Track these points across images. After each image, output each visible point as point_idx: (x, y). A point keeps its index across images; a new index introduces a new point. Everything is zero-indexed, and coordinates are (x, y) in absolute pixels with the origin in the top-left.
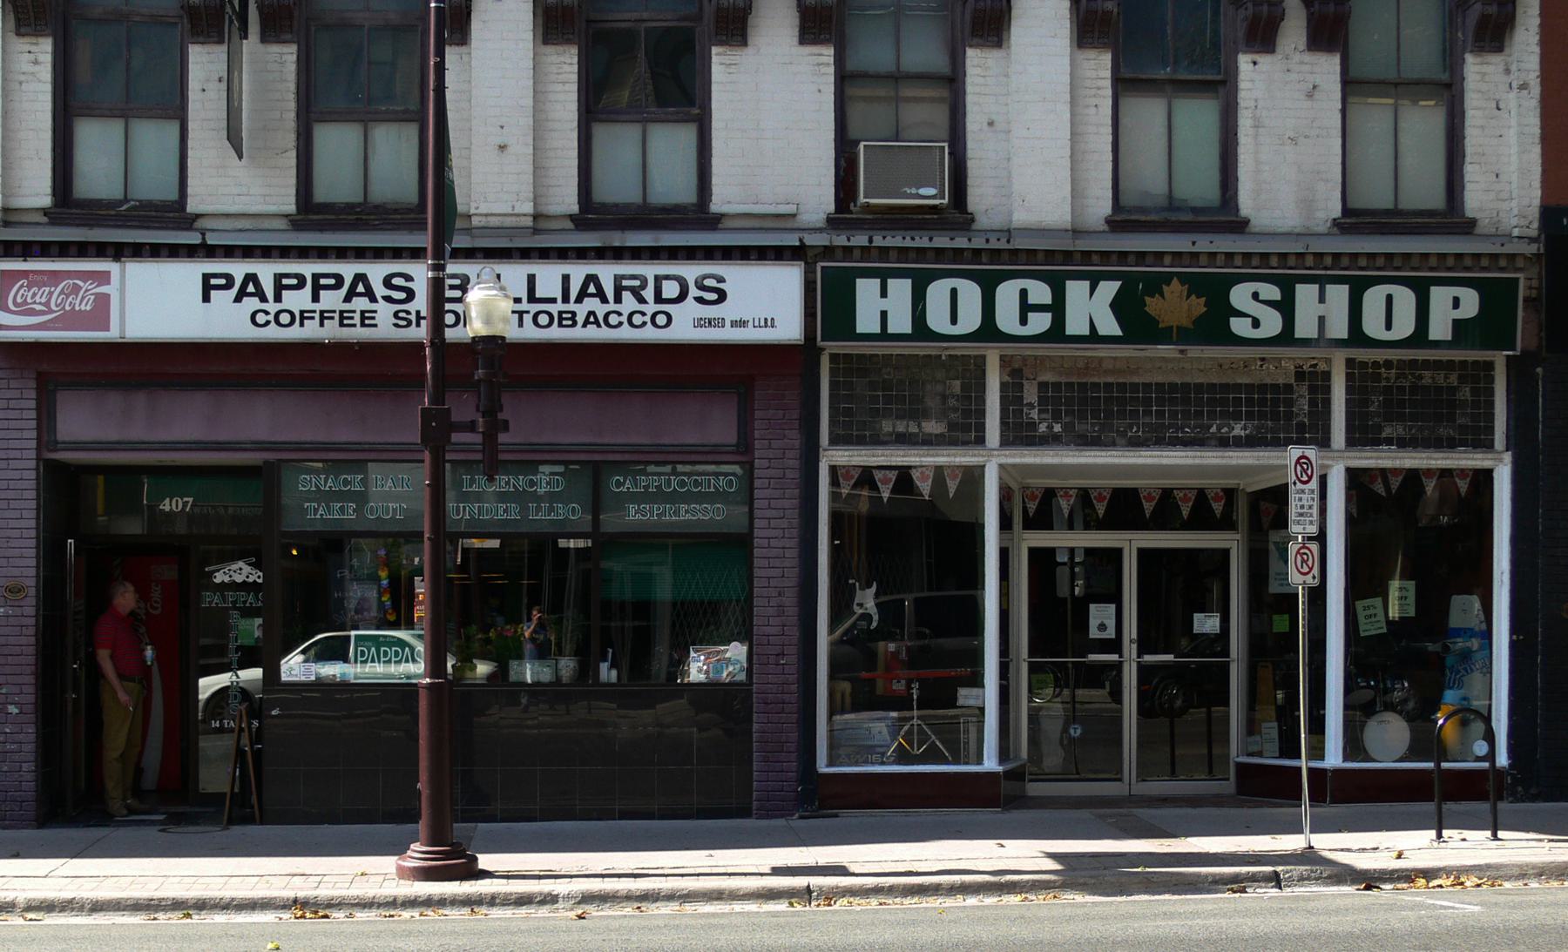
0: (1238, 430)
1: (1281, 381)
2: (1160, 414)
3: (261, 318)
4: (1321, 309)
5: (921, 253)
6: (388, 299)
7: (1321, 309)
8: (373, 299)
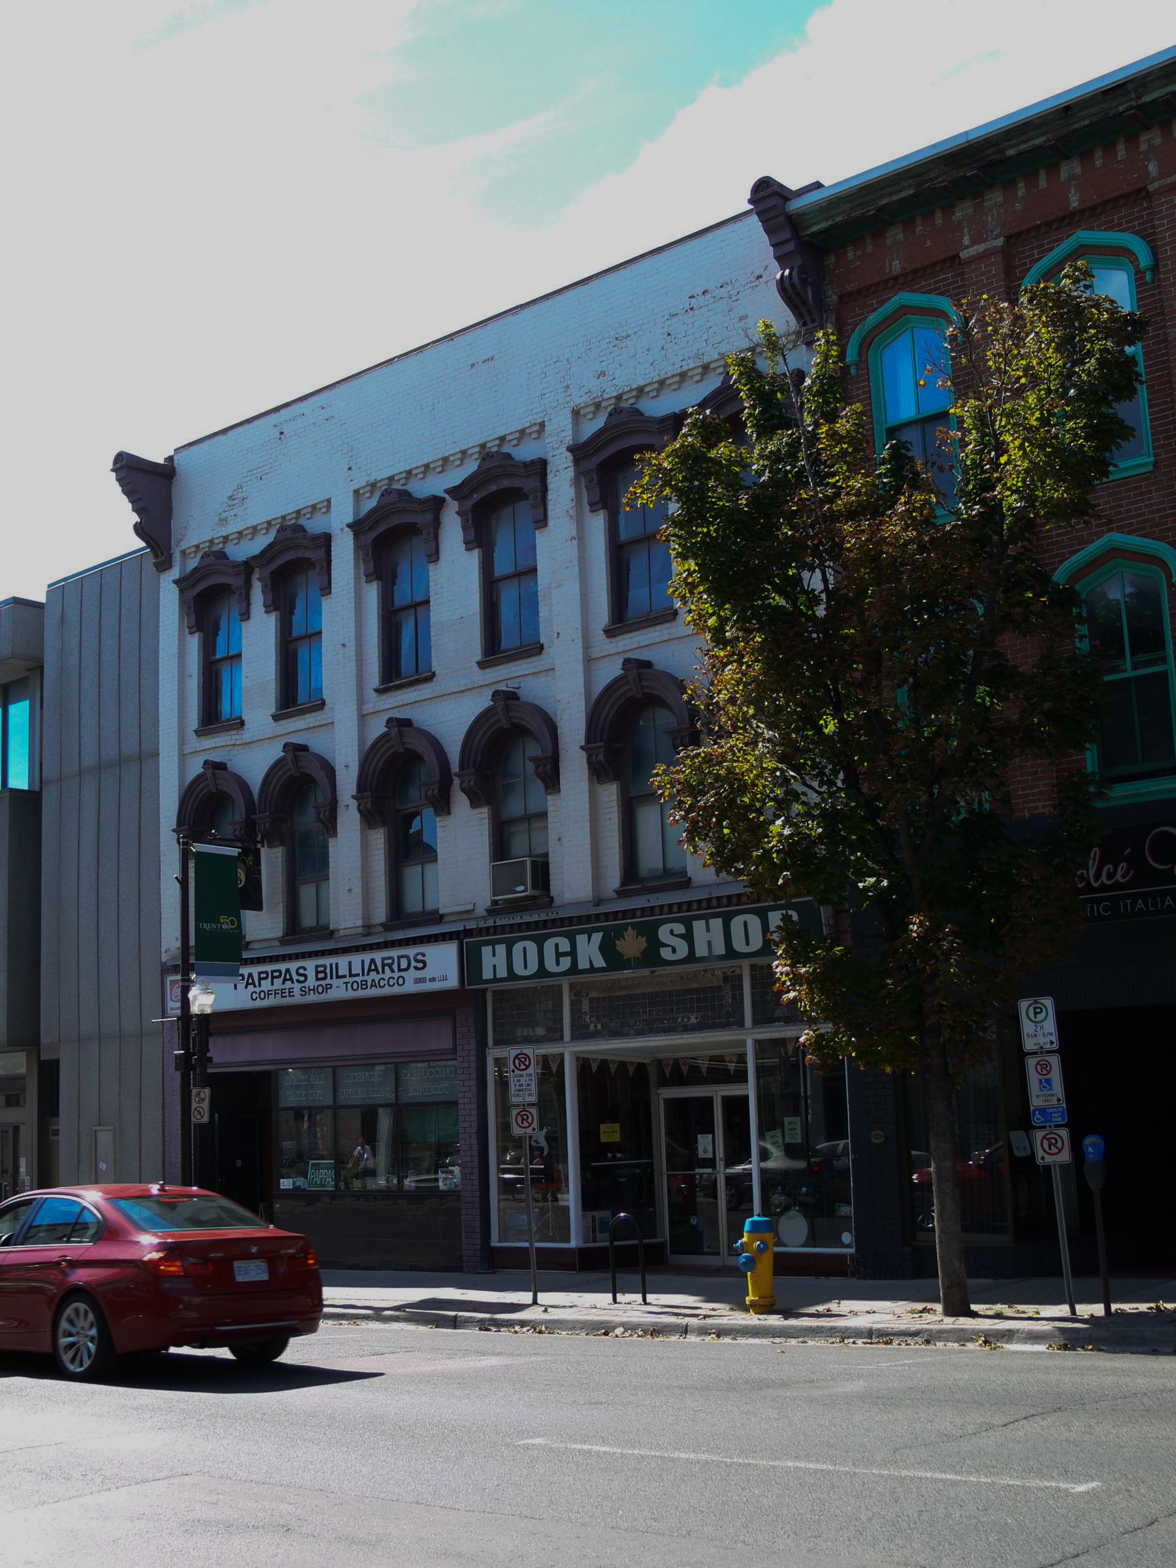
0: (693, 1020)
1: (715, 984)
2: (651, 1012)
3: (254, 996)
4: (707, 936)
5: (536, 925)
6: (298, 981)
7: (707, 936)
8: (293, 982)
